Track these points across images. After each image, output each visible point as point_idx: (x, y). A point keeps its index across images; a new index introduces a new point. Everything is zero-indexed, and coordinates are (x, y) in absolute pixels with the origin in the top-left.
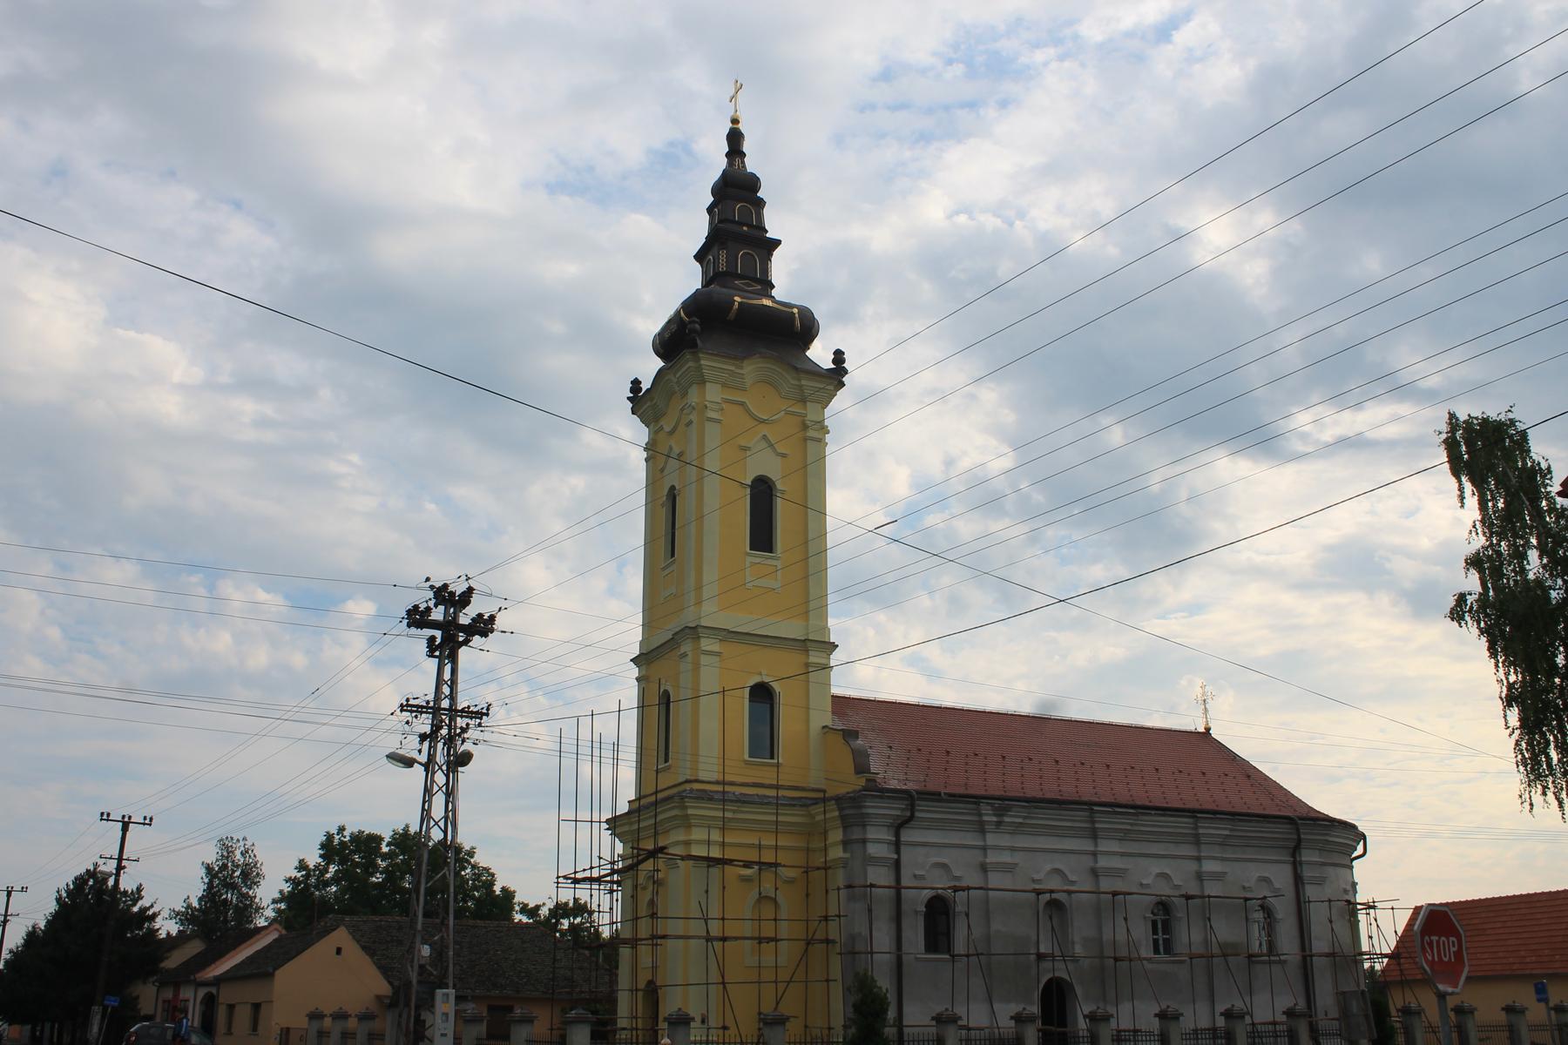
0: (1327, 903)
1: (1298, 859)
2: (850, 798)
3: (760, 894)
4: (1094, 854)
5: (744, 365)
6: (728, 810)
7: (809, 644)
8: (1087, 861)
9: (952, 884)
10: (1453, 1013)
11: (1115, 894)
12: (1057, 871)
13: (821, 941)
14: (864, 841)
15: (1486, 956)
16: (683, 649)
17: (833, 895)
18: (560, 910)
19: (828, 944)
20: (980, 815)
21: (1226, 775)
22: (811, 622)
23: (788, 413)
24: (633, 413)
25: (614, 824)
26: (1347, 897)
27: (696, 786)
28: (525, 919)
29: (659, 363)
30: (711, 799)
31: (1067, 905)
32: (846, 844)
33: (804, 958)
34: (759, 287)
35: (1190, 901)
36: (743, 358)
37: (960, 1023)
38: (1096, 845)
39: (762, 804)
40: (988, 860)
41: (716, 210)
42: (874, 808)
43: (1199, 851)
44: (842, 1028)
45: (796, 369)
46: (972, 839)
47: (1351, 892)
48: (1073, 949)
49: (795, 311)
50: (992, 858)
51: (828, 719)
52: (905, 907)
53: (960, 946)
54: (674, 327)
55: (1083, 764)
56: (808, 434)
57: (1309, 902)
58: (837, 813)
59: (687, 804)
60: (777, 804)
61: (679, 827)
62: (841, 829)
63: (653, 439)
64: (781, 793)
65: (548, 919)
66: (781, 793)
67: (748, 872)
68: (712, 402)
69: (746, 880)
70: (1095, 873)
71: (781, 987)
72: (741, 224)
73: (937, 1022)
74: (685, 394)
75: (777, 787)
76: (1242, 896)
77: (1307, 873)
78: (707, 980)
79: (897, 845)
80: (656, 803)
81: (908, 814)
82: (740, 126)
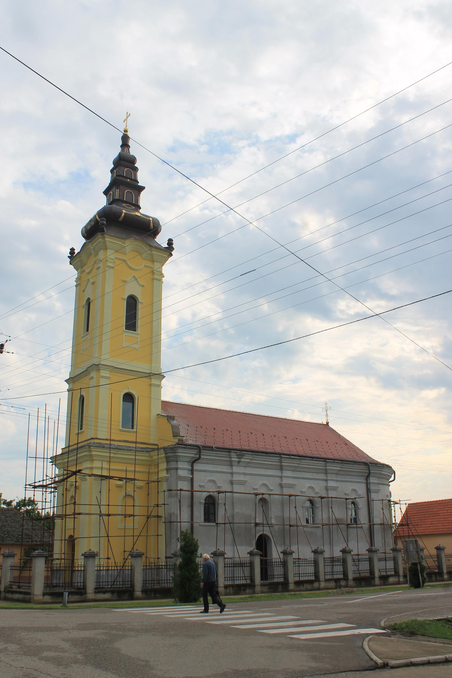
0: (382, 501)
1: (368, 481)
2: (171, 448)
3: (126, 493)
4: (281, 477)
6: (113, 453)
8: (278, 480)
9: (217, 490)
10: (282, 554)
11: (290, 496)
12: (264, 485)
13: (155, 517)
14: (177, 469)
16: (91, 375)
17: (161, 495)
18: (23, 503)
19: (158, 517)
20: (231, 458)
21: (337, 443)
22: (152, 365)
24: (70, 264)
25: (54, 460)
26: (388, 499)
27: (96, 441)
28: (5, 507)
29: (83, 241)
30: (103, 447)
31: (269, 500)
32: (168, 470)
34: (134, 208)
35: (323, 499)
38: (282, 473)
39: (127, 450)
40: (234, 479)
41: (115, 171)
42: (181, 453)
43: (327, 477)
44: (165, 558)
45: (150, 246)
46: (226, 469)
47: (389, 496)
48: (271, 521)
49: (151, 219)
50: (236, 478)
51: (159, 411)
52: (195, 500)
53: (220, 519)
54: (93, 223)
55: (275, 436)
56: (154, 277)
57: (373, 500)
58: (164, 455)
59: (92, 449)
60: (136, 451)
61: (87, 460)
62: (166, 463)
63: (79, 276)
65: (16, 507)
67: (120, 483)
69: (119, 486)
70: (281, 486)
71: (136, 538)
74: (97, 254)
75: (136, 443)
76: (345, 497)
77: (372, 487)
78: (100, 535)
79: (192, 471)
80: (77, 449)
81: (198, 456)
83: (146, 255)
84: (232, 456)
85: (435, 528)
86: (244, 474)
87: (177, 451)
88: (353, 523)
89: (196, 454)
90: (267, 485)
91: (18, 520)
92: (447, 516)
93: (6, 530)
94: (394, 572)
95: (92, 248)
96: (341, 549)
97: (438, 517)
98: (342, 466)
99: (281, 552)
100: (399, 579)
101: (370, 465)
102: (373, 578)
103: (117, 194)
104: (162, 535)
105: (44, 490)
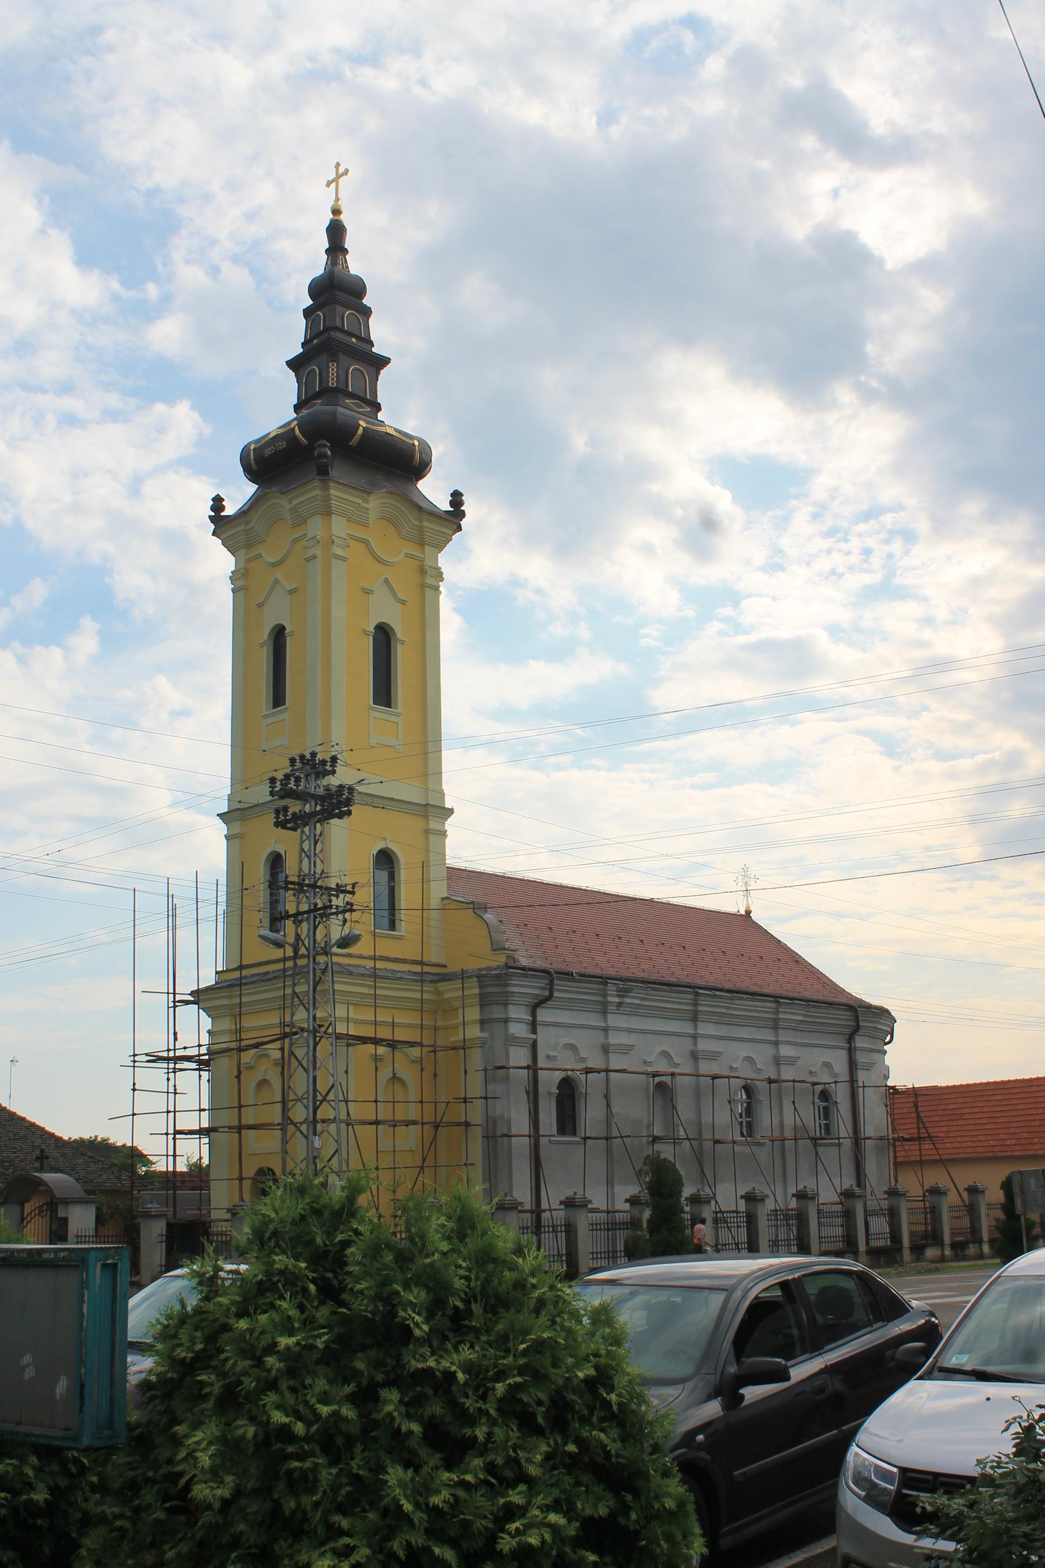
5: (371, 499)
7: (430, 809)
10: (966, 1192)
11: (714, 1077)
12: (665, 1054)
14: (506, 1021)
15: (966, 1139)
20: (605, 995)
23: (407, 556)
32: (482, 1022)
33: (434, 1143)
36: (369, 493)
37: (590, 1206)
38: (696, 1028)
43: (777, 1036)
49: (416, 443)
52: (541, 1089)
56: (426, 581)
57: (864, 1087)
58: (477, 991)
59: (700, 1002)
62: (478, 1008)
64: (245, 972)
66: (426, 969)
68: (339, 537)
72: (352, 335)
73: (565, 1206)
77: (860, 1058)
79: (534, 1026)
81: (547, 993)
82: (342, 217)
83: (410, 528)
84: (609, 992)
85: (956, 1145)
86: (628, 1032)
87: (509, 982)
88: (823, 1134)
89: (542, 989)
90: (668, 1053)
91: (22, 1133)
92: (982, 1121)
93: (6, 1157)
94: (795, 1247)
95: (288, 507)
96: (628, 1197)
97: (960, 1122)
98: (807, 1012)
99: (742, 1197)
100: (943, 1250)
101: (859, 1009)
102: (900, 1250)
103: (333, 374)
104: (473, 1164)
105: (172, 1066)
